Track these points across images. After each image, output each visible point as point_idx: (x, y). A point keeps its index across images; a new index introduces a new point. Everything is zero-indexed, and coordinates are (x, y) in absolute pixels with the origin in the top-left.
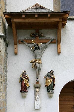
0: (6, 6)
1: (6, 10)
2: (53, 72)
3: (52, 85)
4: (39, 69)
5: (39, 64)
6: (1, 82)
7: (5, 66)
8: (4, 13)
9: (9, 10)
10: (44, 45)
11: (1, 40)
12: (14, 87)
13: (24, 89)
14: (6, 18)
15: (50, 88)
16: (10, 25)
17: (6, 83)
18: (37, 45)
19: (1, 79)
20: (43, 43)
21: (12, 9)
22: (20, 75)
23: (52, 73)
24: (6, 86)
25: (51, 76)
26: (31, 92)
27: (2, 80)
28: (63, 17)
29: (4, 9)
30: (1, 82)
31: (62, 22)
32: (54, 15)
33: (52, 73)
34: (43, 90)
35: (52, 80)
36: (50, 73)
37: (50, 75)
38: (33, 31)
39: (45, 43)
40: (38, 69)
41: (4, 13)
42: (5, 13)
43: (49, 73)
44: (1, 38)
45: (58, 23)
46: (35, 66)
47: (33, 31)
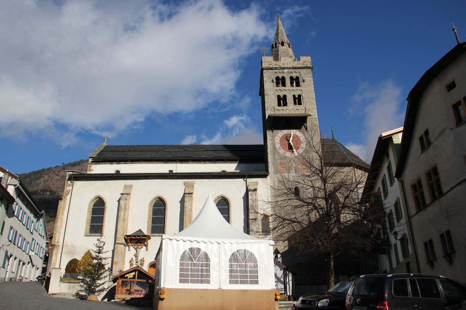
22: (130, 259)
23: (143, 258)
33: (143, 258)
46: (136, 256)
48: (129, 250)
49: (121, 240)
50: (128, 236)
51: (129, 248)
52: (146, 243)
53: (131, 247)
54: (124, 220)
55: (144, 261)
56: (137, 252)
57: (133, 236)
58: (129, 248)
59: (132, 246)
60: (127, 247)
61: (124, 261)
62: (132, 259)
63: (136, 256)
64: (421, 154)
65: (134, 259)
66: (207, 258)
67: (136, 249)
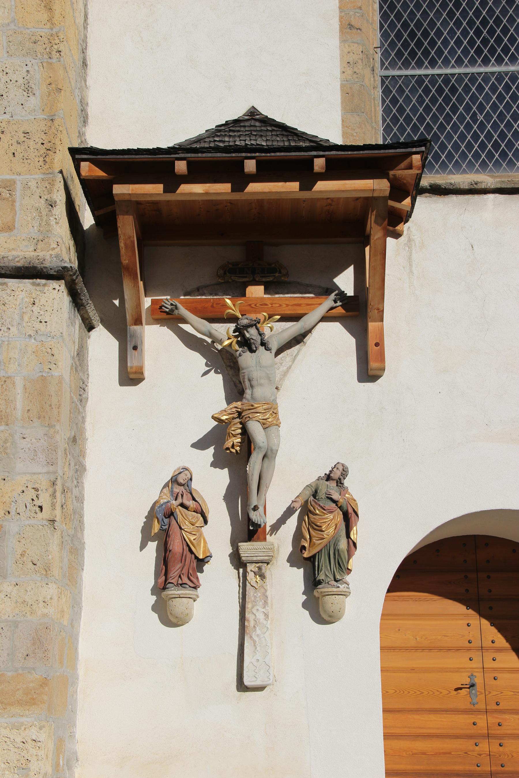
0: (85, 122)
1: (81, 135)
2: (345, 472)
3: (343, 545)
5: (265, 426)
6: (54, 521)
7: (74, 440)
8: (73, 151)
10: (291, 329)
12: (118, 564)
13: (176, 567)
14: (85, 183)
15: (321, 567)
16: (106, 221)
18: (255, 324)
20: (284, 318)
22: (151, 492)
23: (336, 477)
25: (336, 496)
26: (219, 578)
28: (391, 173)
30: (54, 521)
31: (391, 203)
32: (347, 161)
33: (336, 477)
34: (287, 582)
35: (339, 517)
36: (328, 478)
39: (296, 318)
40: (261, 456)
41: (73, 151)
43: (319, 478)
45: (368, 202)
46: (237, 448)
47: (234, 253)
48: (130, 377)
49: (27, 224)
50: (94, 155)
51: (128, 345)
52: (345, 281)
53: (157, 341)
54: (476, 184)
55: (349, 517)
56: (236, 389)
57: (199, 172)
58: (128, 345)
59: (169, 318)
60: (103, 344)
61: (76, 518)
62: (180, 483)
63: (237, 448)
64: (268, 685)
65: (212, 484)
66: (143, 379)
67: (226, 364)
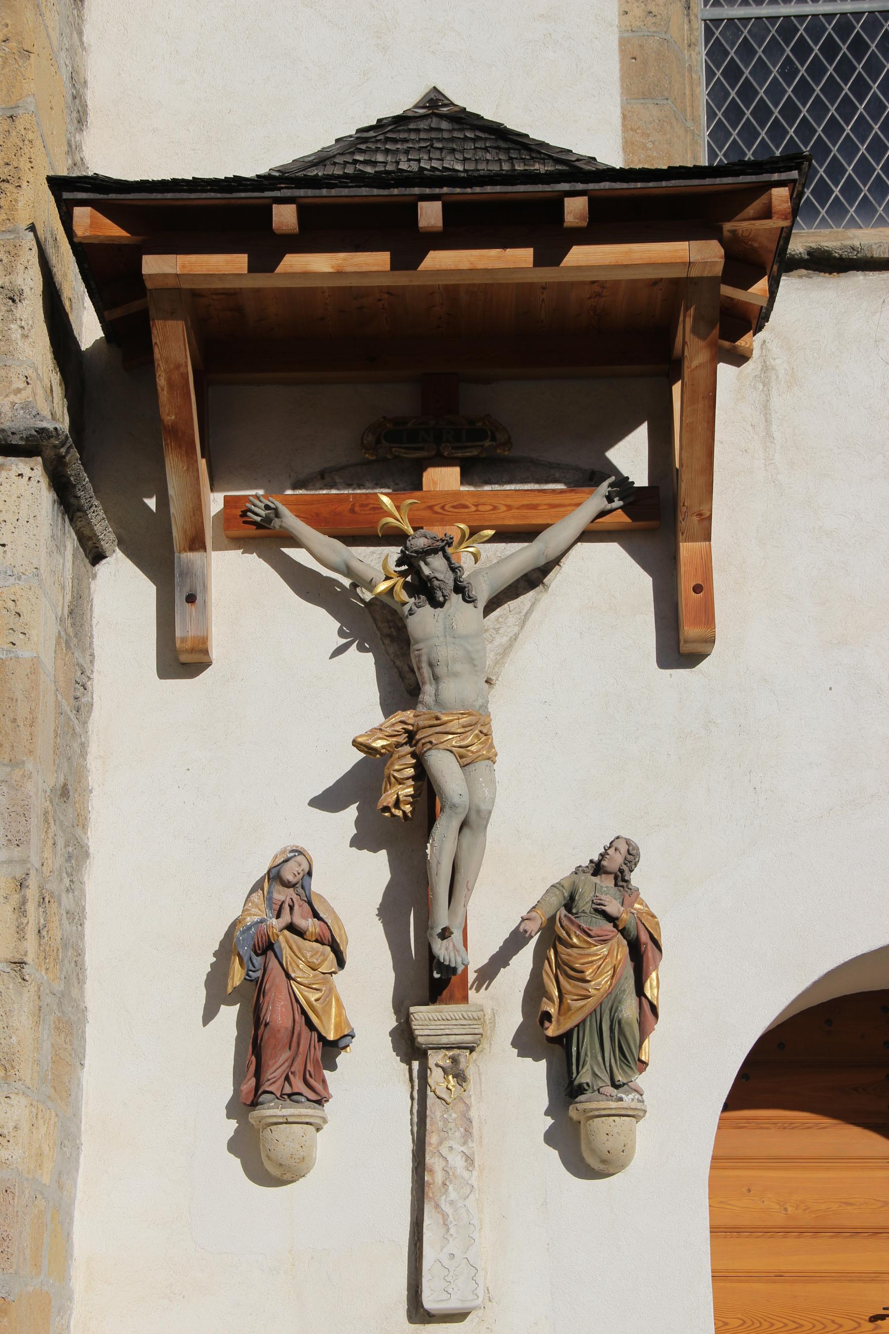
0: (81, 121)
1: (73, 149)
2: (632, 857)
4: (464, 825)
5: (465, 761)
6: (21, 963)
7: (65, 792)
9: (115, 156)
10: (516, 557)
11: (24, 486)
12: (156, 1053)
13: (278, 1058)
14: (81, 250)
15: (584, 1056)
16: (129, 331)
17: (75, 993)
19: (20, 930)
20: (504, 535)
21: (146, 139)
22: (225, 901)
23: (614, 867)
24: (66, 1023)
25: (613, 907)
26: (368, 1083)
27: (31, 945)
29: (59, 150)
30: (21, 963)
31: (727, 291)
32: (635, 203)
33: (614, 867)
35: (622, 951)
36: (597, 869)
37: (597, 928)
38: (398, 399)
39: (528, 534)
42: (68, 190)
43: (578, 870)
44: (19, 465)
45: (677, 289)
46: (405, 807)
47: (398, 399)
